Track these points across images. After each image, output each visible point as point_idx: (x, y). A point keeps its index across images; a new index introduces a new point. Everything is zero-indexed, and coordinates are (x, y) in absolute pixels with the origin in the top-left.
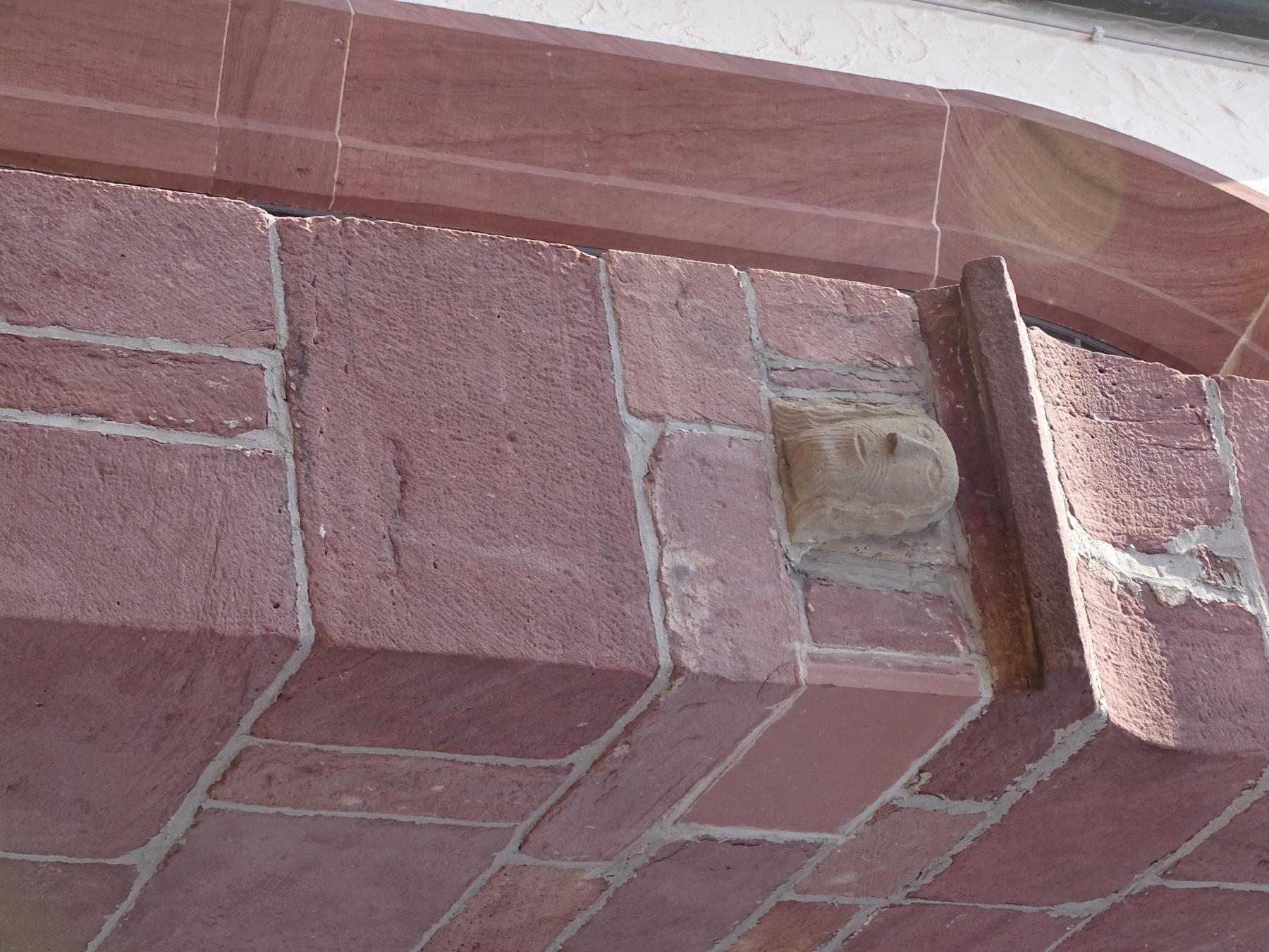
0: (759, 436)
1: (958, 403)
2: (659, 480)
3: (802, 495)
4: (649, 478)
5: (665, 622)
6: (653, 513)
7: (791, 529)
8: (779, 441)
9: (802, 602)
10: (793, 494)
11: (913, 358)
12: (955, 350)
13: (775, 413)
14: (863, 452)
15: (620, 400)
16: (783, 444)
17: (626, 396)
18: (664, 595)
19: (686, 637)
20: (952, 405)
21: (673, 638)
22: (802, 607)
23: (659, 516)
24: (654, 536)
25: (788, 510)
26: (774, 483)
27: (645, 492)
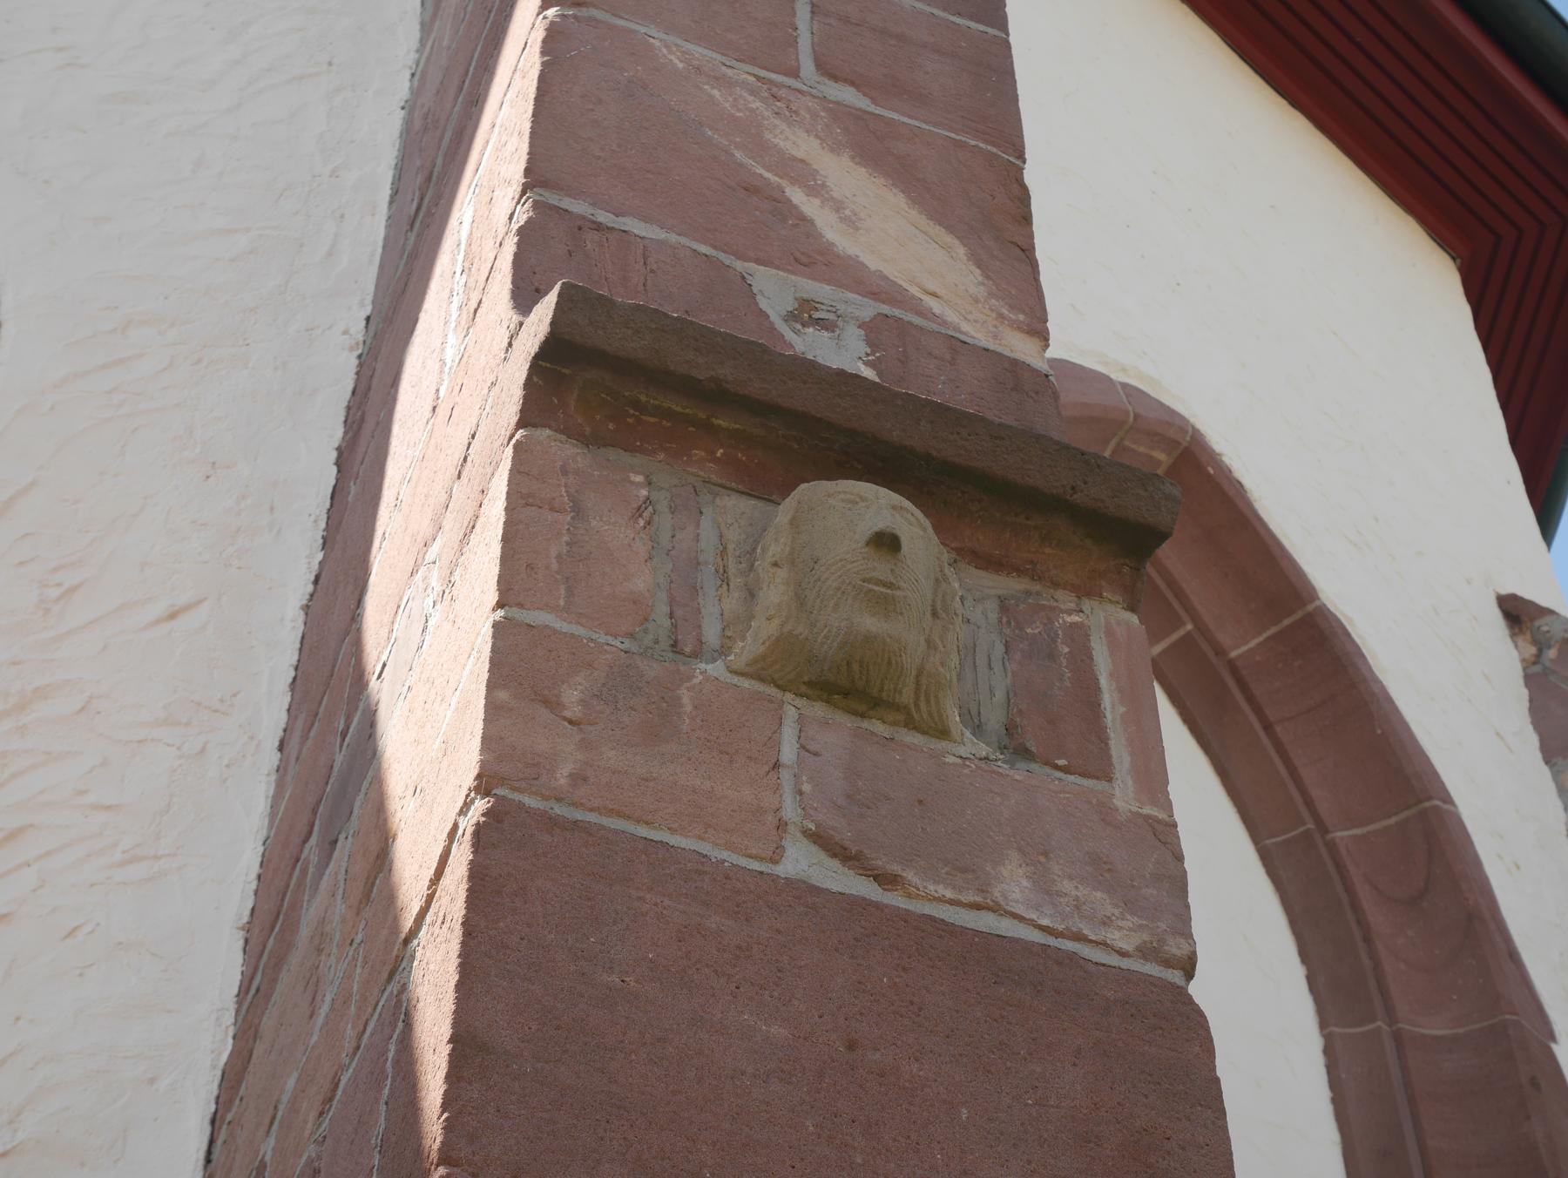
0: (790, 713)
1: (714, 453)
2: (896, 868)
3: (906, 697)
4: (887, 880)
5: (1123, 954)
6: (941, 900)
7: (943, 733)
8: (803, 689)
9: (1047, 769)
10: (897, 707)
11: (638, 473)
12: (632, 416)
13: (758, 671)
14: (890, 586)
15: (755, 866)
16: (810, 684)
17: (751, 857)
18: (1079, 937)
19: (1146, 937)
20: (716, 460)
21: (1144, 952)
22: (1059, 774)
23: (949, 894)
24: (984, 913)
25: (911, 724)
26: (865, 724)
27: (909, 896)
